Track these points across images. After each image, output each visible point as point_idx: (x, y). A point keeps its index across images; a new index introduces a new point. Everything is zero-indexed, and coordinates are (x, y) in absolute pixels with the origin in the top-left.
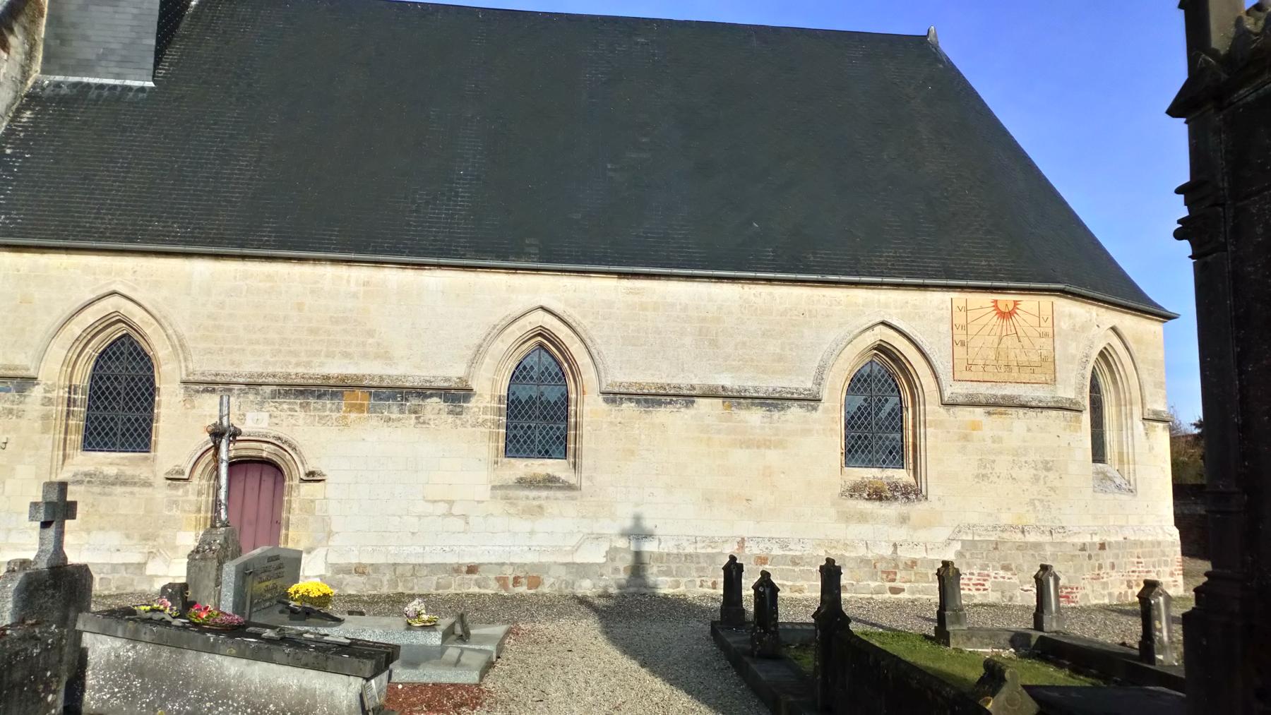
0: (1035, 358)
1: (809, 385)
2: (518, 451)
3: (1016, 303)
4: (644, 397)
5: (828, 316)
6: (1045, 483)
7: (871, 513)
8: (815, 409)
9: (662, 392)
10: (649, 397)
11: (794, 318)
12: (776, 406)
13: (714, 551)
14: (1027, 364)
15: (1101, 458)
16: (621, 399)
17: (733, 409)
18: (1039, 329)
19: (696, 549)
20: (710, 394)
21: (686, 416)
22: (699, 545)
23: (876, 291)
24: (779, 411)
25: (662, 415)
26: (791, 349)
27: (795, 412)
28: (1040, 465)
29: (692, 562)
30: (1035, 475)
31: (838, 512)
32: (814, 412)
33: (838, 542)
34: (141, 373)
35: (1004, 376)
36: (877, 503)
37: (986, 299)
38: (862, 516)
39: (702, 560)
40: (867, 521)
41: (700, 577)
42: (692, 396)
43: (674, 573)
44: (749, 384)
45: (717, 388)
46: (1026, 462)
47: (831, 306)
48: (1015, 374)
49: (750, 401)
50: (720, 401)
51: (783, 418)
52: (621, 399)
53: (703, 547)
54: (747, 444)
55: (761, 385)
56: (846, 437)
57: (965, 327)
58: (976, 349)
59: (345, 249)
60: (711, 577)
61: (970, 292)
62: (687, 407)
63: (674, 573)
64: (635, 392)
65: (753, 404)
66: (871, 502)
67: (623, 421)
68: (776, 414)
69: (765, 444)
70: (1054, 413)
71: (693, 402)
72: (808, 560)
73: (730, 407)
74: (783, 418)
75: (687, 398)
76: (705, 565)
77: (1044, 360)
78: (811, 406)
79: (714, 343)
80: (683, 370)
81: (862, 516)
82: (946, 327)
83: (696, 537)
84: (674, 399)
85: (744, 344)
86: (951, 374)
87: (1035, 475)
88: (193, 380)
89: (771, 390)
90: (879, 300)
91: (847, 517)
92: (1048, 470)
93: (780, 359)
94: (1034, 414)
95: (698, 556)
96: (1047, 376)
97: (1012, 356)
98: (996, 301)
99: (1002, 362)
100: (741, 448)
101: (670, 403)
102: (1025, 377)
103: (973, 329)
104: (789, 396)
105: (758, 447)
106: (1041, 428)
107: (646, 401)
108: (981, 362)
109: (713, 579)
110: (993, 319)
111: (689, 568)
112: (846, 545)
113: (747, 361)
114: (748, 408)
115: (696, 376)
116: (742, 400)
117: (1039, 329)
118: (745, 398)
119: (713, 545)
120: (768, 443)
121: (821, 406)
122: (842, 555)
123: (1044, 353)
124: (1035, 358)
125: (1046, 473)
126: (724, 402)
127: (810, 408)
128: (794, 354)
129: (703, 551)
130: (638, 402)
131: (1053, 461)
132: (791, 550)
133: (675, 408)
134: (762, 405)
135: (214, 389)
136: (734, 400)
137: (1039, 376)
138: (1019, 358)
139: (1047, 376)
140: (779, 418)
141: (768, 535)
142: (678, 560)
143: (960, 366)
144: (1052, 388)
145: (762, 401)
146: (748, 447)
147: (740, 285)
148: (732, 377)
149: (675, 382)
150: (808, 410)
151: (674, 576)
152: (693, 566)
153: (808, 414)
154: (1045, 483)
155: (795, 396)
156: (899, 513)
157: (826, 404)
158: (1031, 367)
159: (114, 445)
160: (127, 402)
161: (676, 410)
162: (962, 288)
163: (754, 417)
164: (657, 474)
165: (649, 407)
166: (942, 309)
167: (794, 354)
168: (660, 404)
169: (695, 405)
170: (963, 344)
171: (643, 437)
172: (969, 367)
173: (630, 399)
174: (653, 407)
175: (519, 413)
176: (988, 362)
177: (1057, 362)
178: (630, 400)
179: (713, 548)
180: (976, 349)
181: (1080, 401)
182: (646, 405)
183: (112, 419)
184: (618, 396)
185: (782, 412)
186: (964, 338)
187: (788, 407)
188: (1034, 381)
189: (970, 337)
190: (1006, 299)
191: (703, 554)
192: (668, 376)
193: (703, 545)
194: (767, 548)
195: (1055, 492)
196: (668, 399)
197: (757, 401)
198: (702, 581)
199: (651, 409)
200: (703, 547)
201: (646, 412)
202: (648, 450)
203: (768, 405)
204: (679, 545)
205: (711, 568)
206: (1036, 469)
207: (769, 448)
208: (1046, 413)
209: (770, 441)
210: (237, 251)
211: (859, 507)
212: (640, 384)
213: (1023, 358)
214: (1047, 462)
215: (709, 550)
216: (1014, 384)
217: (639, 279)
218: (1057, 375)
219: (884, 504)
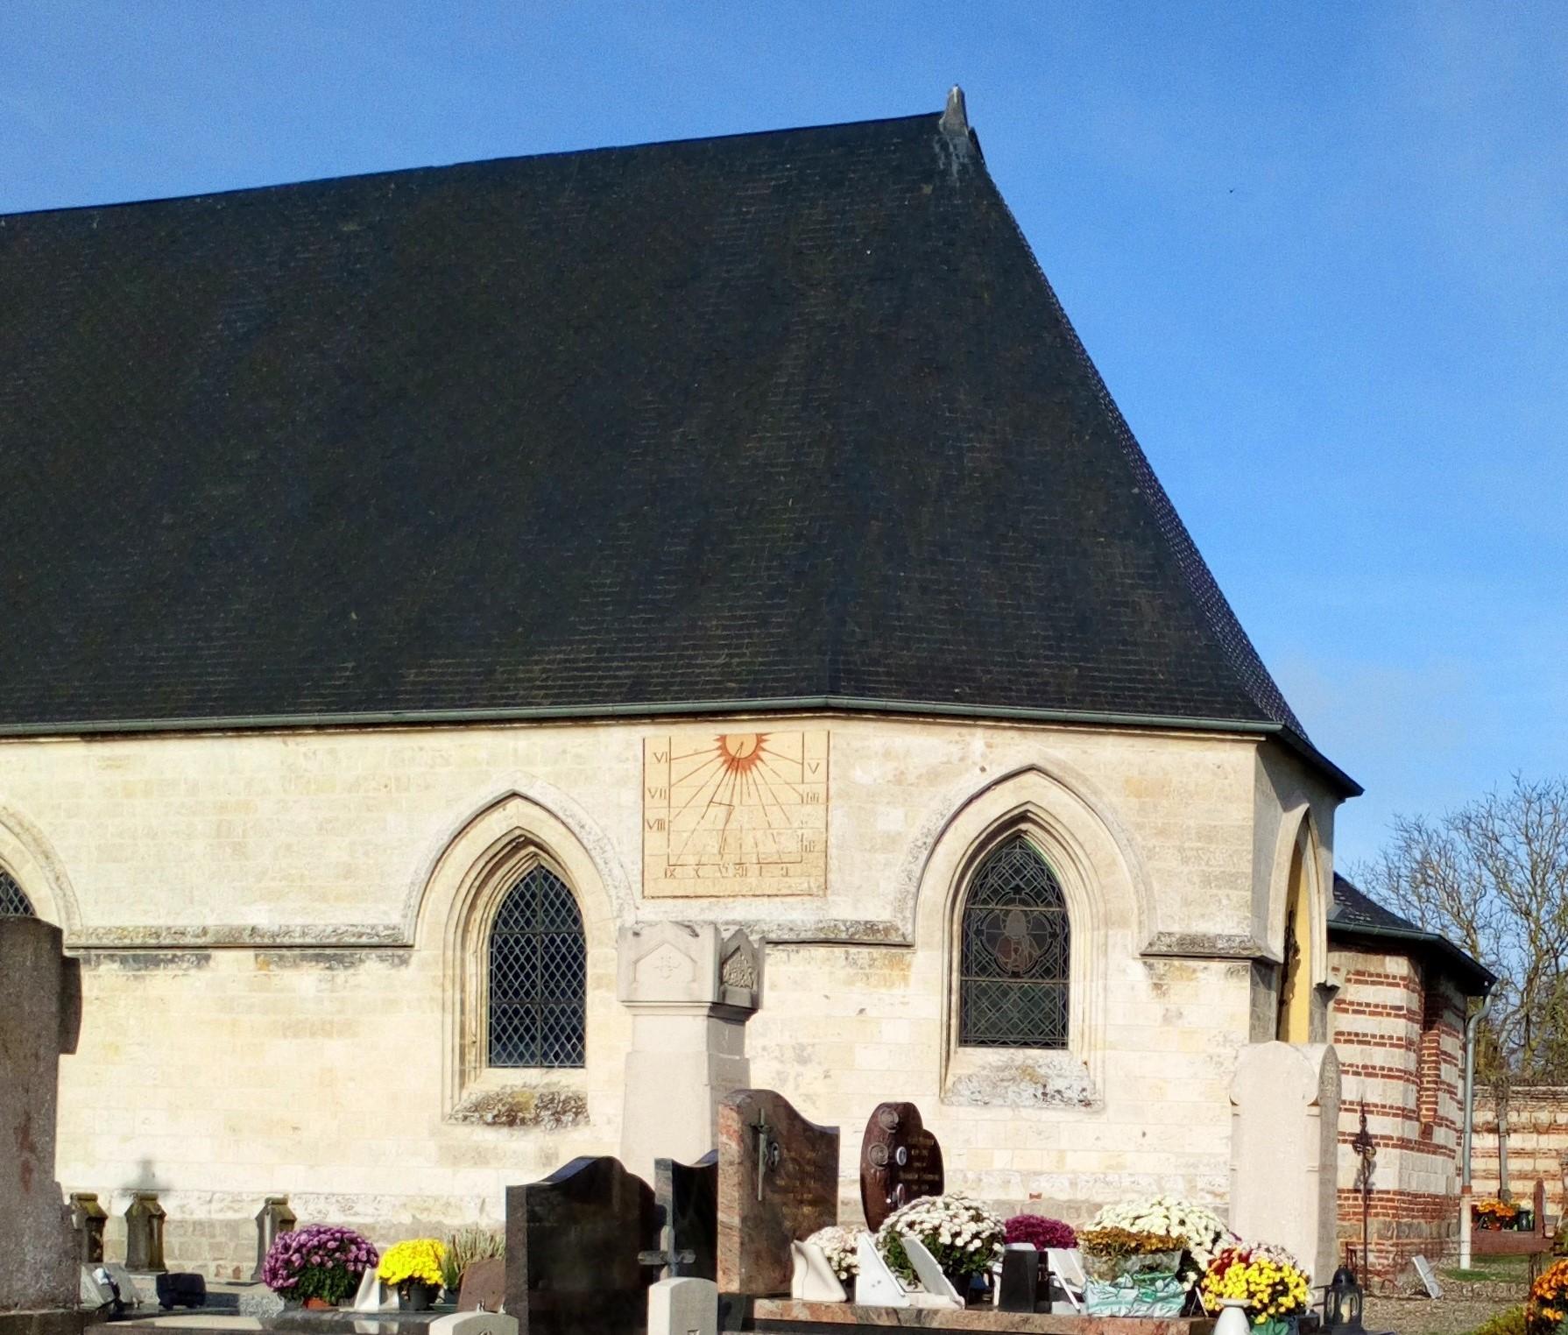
0: (791, 845)
1: (395, 919)
2: (510, 1055)
3: (760, 739)
4: (132, 952)
5: (427, 788)
6: (797, 1087)
7: (495, 1148)
8: (404, 962)
9: (152, 942)
10: (139, 952)
11: (371, 794)
12: (340, 960)
13: (237, 1216)
14: (775, 858)
15: (972, 1036)
16: (98, 956)
17: (272, 967)
18: (800, 788)
19: (210, 1212)
20: (230, 943)
21: (198, 984)
22: (215, 1206)
23: (510, 734)
24: (346, 968)
25: (162, 981)
26: (366, 854)
27: (372, 968)
28: (789, 1054)
29: (203, 1235)
30: (779, 1073)
31: (441, 1148)
32: (403, 968)
33: (436, 1200)
34: (553, 929)
35: (731, 885)
36: (505, 1130)
37: (703, 736)
38: (479, 1153)
39: (218, 1231)
40: (487, 1163)
41: (215, 1259)
42: (206, 947)
43: (177, 1252)
44: (297, 922)
45: (241, 930)
46: (764, 1049)
47: (432, 767)
48: (752, 880)
49: (297, 952)
50: (251, 953)
51: (352, 981)
52: (98, 956)
53: (221, 1210)
54: (293, 1029)
55: (317, 922)
56: (492, 1012)
57: (667, 794)
58: (685, 835)
59: (920, 692)
60: (233, 1260)
61: (181, 738)
62: (199, 966)
63: (177, 1252)
64: (111, 944)
65: (304, 958)
66: (494, 1128)
67: (102, 995)
68: (341, 974)
69: (325, 1029)
70: (821, 952)
71: (208, 958)
72: (383, 1232)
73: (267, 963)
74: (352, 981)
75: (200, 950)
76: (223, 1239)
77: (807, 849)
78: (399, 956)
79: (239, 849)
80: (192, 901)
81: (479, 1153)
82: (630, 796)
83: (214, 1193)
84: (179, 953)
85: (289, 847)
86: (640, 885)
87: (779, 1073)
88: (120, 945)
89: (330, 929)
90: (516, 750)
91: (454, 1157)
92: (803, 1061)
93: (349, 873)
94: (784, 955)
95: (212, 1224)
96: (812, 880)
97: (749, 842)
98: (723, 738)
99: (731, 857)
100: (285, 1036)
101: (172, 961)
102: (769, 884)
103: (680, 795)
104: (353, 940)
105: (313, 1034)
106: (795, 982)
107: (136, 958)
108: (692, 860)
109: (235, 1264)
110: (715, 769)
111: (199, 1245)
112: (448, 1204)
113: (293, 881)
114: (295, 965)
115: (212, 911)
116: (284, 952)
117: (800, 788)
118: (290, 947)
119: (236, 1206)
120: (328, 1027)
121: (416, 957)
122: (439, 1223)
123: (808, 834)
124: (791, 845)
125: (801, 1069)
126: (257, 956)
127: (396, 961)
128: (371, 862)
129: (221, 1216)
130: (124, 960)
131: (813, 1045)
132: (356, 1214)
133: (180, 969)
134: (317, 958)
135: (175, 956)
136: (273, 952)
137: (797, 880)
138: (761, 848)
139: (812, 880)
140: (346, 982)
141: (326, 1190)
142: (182, 1232)
143: (656, 868)
144: (818, 903)
145: (317, 951)
146: (296, 1036)
147: (280, 739)
148: (271, 910)
149: (180, 922)
150: (393, 965)
151: (176, 1259)
152: (205, 1241)
153: (393, 972)
154: (797, 1087)
155: (364, 940)
156: (541, 1149)
157: (424, 953)
158: (782, 864)
159: (521, 1056)
160: (499, 981)
161: (180, 973)
162: (653, 717)
163: (306, 979)
164: (155, 1086)
165: (139, 970)
166: (628, 759)
167: (371, 862)
168: (156, 962)
169: (212, 963)
170: (661, 825)
171: (132, 1022)
172: (670, 871)
173: (112, 956)
174: (147, 968)
175: (522, 987)
176: (704, 860)
177: (833, 851)
178: (111, 958)
179: (235, 1211)
180: (685, 835)
181: (900, 925)
182: (136, 966)
183: (528, 1012)
184: (93, 952)
185: (351, 971)
186: (663, 814)
187: (361, 961)
188: (785, 891)
189: (674, 812)
190: (742, 732)
191: (221, 1221)
192: (169, 913)
193: (222, 1205)
194: (319, 1212)
195: (814, 1103)
196: (170, 953)
197: (310, 952)
198: (218, 1266)
199: (143, 972)
200: (221, 1210)
201: (136, 977)
202: (140, 1044)
203: (329, 958)
204: (184, 1206)
205: (232, 1245)
206: (782, 1062)
207: (329, 1035)
208: (805, 951)
209: (331, 1023)
210: (385, 716)
211: (475, 1138)
212: (123, 929)
213: (769, 848)
214: (802, 1048)
215: (230, 1215)
216: (749, 900)
217: (114, 740)
218: (831, 877)
219: (517, 1132)
